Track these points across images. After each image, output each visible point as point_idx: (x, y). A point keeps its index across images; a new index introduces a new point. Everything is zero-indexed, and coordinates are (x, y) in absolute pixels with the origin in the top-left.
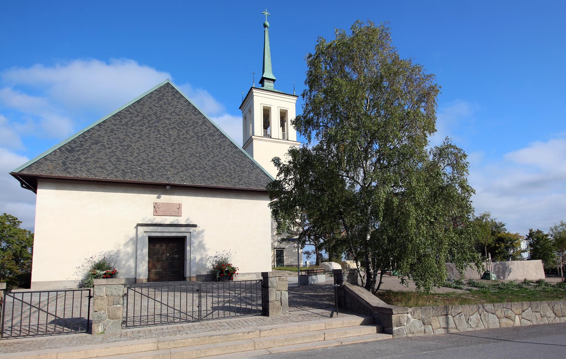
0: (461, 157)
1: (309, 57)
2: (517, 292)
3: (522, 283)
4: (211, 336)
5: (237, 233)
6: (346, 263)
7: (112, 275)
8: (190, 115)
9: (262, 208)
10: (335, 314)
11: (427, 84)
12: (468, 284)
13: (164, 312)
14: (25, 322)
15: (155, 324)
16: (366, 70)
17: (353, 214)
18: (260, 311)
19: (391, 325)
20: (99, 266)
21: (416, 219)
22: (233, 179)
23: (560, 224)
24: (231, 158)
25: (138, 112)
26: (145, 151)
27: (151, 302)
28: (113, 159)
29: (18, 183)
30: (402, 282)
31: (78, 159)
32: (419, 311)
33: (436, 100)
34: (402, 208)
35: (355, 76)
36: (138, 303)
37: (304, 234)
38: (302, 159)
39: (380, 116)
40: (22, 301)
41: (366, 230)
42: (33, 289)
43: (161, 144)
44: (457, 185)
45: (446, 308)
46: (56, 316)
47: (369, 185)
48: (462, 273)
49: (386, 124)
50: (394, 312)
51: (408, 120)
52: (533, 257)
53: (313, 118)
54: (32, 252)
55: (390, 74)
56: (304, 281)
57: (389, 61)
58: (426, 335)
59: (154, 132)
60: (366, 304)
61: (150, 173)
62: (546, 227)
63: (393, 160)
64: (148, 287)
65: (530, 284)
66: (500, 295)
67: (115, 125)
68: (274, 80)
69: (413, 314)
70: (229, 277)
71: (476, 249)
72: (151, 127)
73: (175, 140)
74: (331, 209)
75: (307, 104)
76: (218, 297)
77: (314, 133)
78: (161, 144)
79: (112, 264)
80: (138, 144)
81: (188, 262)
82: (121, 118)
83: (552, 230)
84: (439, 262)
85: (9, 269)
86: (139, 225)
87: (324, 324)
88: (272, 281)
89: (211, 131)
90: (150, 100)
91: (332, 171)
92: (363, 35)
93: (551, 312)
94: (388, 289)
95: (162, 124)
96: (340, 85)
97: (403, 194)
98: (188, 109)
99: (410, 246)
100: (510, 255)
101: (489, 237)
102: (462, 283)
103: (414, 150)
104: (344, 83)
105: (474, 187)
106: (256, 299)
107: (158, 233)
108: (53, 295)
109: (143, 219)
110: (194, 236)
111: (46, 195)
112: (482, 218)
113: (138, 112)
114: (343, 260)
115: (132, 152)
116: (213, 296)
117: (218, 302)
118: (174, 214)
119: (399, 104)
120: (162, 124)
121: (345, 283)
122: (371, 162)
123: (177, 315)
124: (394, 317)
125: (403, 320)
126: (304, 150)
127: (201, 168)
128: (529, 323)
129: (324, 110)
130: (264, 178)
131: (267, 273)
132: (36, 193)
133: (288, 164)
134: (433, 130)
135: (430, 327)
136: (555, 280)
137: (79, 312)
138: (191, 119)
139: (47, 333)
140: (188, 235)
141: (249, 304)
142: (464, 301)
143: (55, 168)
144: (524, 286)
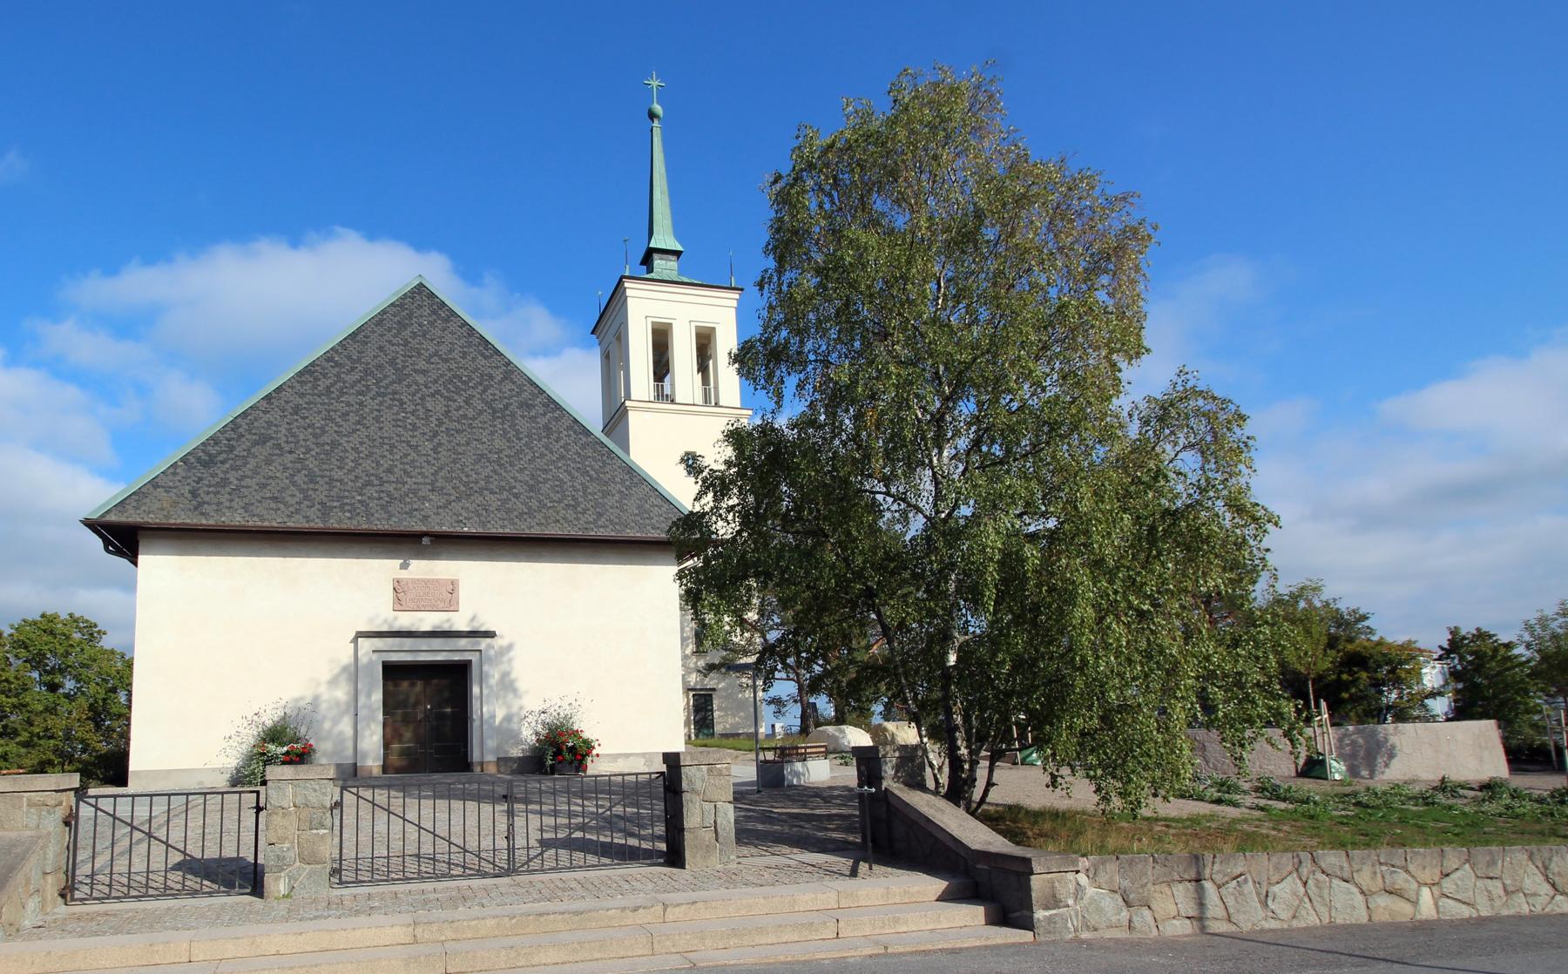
0: (1229, 422)
1: (775, 182)
2: (1419, 816)
3: (1434, 788)
4: (541, 915)
5: (604, 655)
6: (885, 730)
7: (300, 757)
8: (474, 360)
9: (656, 587)
10: (863, 867)
11: (1115, 223)
12: (1257, 790)
13: (427, 849)
14: (121, 866)
15: (406, 880)
16: (931, 201)
17: (905, 596)
18: (660, 854)
19: (1026, 903)
20: (274, 734)
21: (1096, 607)
22: (577, 513)
23: (1556, 609)
24: (574, 461)
25: (354, 362)
26: (371, 454)
27: (397, 824)
28: (300, 478)
29: (98, 542)
30: (1054, 782)
31: (225, 482)
32: (1112, 867)
33: (1143, 265)
34: (1052, 574)
35: (901, 221)
36: (365, 824)
37: (768, 650)
38: (761, 451)
39: (976, 321)
40: (114, 817)
41: (945, 637)
42: (133, 786)
43: (407, 435)
44: (1220, 503)
45: (1196, 859)
46: (184, 853)
47: (949, 515)
48: (1241, 758)
49: (995, 346)
50: (1036, 868)
51: (1062, 328)
52: (1461, 712)
53: (787, 341)
54: (130, 701)
55: (1004, 206)
56: (772, 778)
57: (998, 169)
58: (1136, 936)
59: (390, 407)
60: (950, 844)
61: (383, 507)
62: (1510, 622)
63: (1018, 444)
64: (389, 787)
65: (1461, 792)
66: (1362, 825)
67: (302, 395)
68: (677, 254)
69: (1093, 874)
70: (576, 763)
71: (1284, 688)
72: (384, 395)
73: (440, 423)
74: (843, 584)
75: (771, 307)
76: (555, 814)
77: (791, 382)
78: (407, 435)
79: (303, 730)
80: (355, 439)
81: (476, 724)
82: (317, 379)
83: (1529, 627)
84: (1167, 729)
85: (82, 741)
86: (360, 635)
87: (833, 896)
88: (692, 776)
89: (525, 395)
90: (379, 330)
91: (846, 482)
92: (923, 105)
93: (1540, 878)
94: (1010, 801)
95: (409, 386)
96: (862, 250)
97: (1052, 536)
98: (470, 345)
99: (1079, 683)
100: (1389, 708)
101: (1320, 653)
102: (1237, 789)
103: (1082, 409)
104: (873, 242)
105: (1275, 508)
106: (652, 819)
107: (404, 653)
108: (178, 802)
109: (371, 620)
110: (490, 659)
111: (160, 571)
112: (1295, 598)
113: (354, 362)
114: (876, 720)
115: (342, 459)
116: (541, 813)
117: (556, 828)
118: (441, 605)
119: (1034, 286)
120: (409, 386)
121: (889, 783)
122: (953, 452)
123: (457, 858)
124: (1036, 882)
125: (1063, 891)
126: (766, 430)
127: (502, 489)
128: (1466, 912)
129: (818, 320)
130: (660, 507)
131: (677, 755)
132: (135, 564)
133: (723, 467)
134: (1136, 351)
135: (1146, 912)
136: (1542, 784)
137: (234, 846)
138: (477, 369)
139: (166, 892)
140: (474, 657)
141: (632, 835)
142: (1249, 842)
143: (175, 504)
144: (1440, 798)
